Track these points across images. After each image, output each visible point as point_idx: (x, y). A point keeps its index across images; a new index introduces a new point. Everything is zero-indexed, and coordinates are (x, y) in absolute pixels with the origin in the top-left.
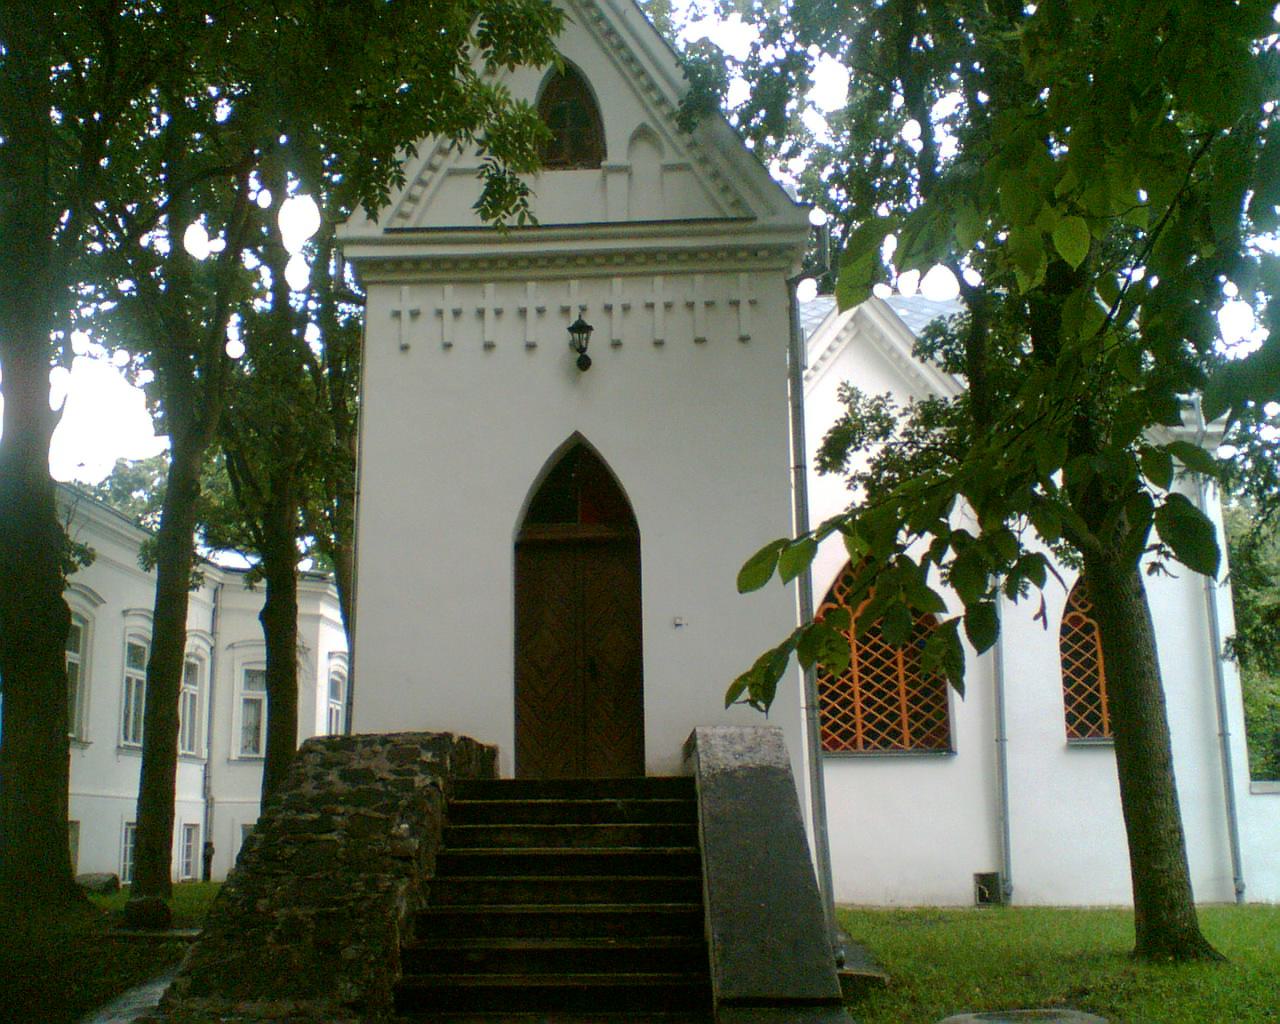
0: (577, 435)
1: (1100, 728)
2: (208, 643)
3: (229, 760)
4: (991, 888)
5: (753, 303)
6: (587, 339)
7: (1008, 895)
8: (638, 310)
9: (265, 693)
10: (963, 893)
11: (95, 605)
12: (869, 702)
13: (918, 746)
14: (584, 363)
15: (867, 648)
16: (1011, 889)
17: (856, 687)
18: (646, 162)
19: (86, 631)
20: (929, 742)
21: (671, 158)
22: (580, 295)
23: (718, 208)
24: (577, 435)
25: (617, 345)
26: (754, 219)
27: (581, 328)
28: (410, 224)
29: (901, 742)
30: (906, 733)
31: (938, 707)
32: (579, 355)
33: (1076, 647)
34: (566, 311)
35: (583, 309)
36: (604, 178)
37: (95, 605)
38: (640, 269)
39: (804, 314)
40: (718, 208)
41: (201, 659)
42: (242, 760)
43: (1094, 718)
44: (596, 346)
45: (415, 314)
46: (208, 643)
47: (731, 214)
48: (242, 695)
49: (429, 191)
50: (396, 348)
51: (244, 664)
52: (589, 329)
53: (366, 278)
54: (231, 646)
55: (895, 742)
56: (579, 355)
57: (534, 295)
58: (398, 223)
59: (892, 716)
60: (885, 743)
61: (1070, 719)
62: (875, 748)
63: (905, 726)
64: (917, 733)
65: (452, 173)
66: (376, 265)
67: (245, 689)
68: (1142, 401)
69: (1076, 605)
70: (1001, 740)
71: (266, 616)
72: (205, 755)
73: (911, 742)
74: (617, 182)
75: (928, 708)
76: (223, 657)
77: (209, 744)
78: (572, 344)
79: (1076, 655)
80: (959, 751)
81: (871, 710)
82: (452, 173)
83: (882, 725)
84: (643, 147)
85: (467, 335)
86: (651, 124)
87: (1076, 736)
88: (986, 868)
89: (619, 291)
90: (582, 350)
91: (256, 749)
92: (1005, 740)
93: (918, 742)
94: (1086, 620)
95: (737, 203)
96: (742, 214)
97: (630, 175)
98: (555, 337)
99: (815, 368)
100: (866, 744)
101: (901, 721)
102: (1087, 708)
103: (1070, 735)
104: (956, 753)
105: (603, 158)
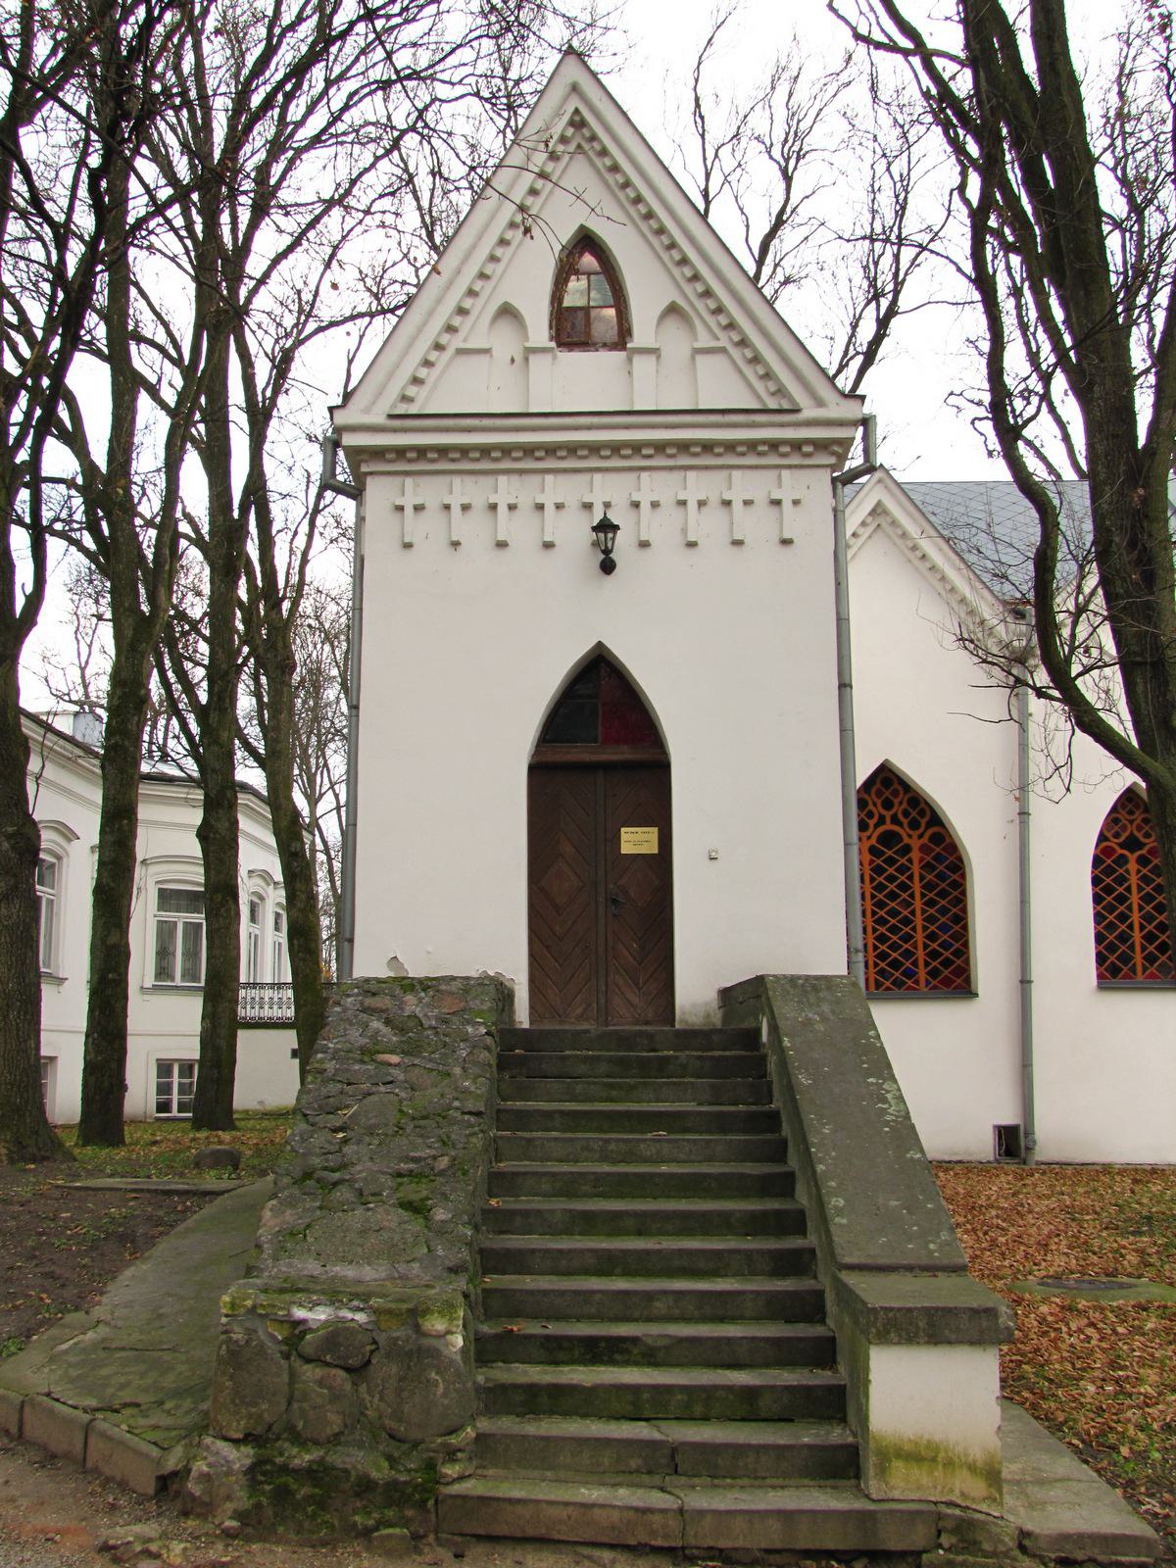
0: (600, 644)
1: (1133, 970)
4: (1012, 1141)
5: (796, 502)
6: (613, 539)
7: (1029, 1149)
8: (478, 513)
10: (983, 1146)
11: (69, 840)
13: (935, 987)
14: (608, 567)
15: (881, 879)
16: (1034, 1142)
18: (676, 342)
19: (60, 868)
20: (947, 982)
21: (704, 341)
22: (610, 490)
23: (758, 397)
24: (600, 644)
25: (644, 545)
26: (797, 411)
27: (606, 527)
28: (413, 409)
29: (917, 982)
30: (922, 973)
31: (957, 945)
32: (603, 556)
33: (890, 853)
34: (588, 506)
35: (607, 505)
36: (630, 360)
37: (69, 840)
38: (671, 462)
40: (758, 397)
43: (1126, 959)
44: (623, 545)
45: (419, 508)
47: (772, 404)
49: (436, 371)
50: (397, 546)
52: (616, 528)
53: (364, 469)
55: (910, 983)
56: (603, 556)
57: (557, 489)
58: (402, 409)
59: (908, 954)
60: (898, 984)
61: (1100, 959)
62: (888, 989)
64: (933, 973)
65: (460, 352)
66: (378, 453)
69: (1109, 835)
70: (1025, 982)
71: (204, 834)
73: (927, 983)
74: (643, 365)
75: (945, 945)
78: (596, 544)
79: (1108, 890)
80: (980, 992)
82: (460, 352)
83: (895, 964)
84: (672, 325)
85: (472, 530)
86: (681, 302)
87: (1105, 978)
88: (1009, 1117)
89: (656, 486)
90: (607, 552)
91: (196, 979)
93: (934, 982)
94: (1120, 851)
95: (781, 391)
96: (786, 406)
97: (659, 357)
98: (574, 533)
101: (917, 960)
102: (1156, 948)
103: (1100, 976)
104: (977, 995)
105: (628, 339)
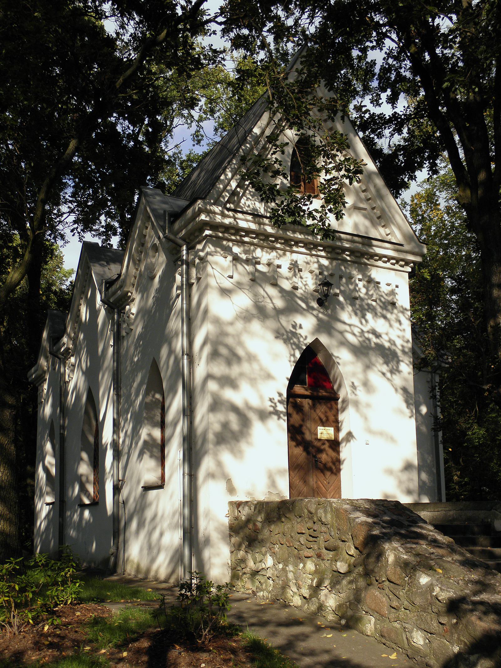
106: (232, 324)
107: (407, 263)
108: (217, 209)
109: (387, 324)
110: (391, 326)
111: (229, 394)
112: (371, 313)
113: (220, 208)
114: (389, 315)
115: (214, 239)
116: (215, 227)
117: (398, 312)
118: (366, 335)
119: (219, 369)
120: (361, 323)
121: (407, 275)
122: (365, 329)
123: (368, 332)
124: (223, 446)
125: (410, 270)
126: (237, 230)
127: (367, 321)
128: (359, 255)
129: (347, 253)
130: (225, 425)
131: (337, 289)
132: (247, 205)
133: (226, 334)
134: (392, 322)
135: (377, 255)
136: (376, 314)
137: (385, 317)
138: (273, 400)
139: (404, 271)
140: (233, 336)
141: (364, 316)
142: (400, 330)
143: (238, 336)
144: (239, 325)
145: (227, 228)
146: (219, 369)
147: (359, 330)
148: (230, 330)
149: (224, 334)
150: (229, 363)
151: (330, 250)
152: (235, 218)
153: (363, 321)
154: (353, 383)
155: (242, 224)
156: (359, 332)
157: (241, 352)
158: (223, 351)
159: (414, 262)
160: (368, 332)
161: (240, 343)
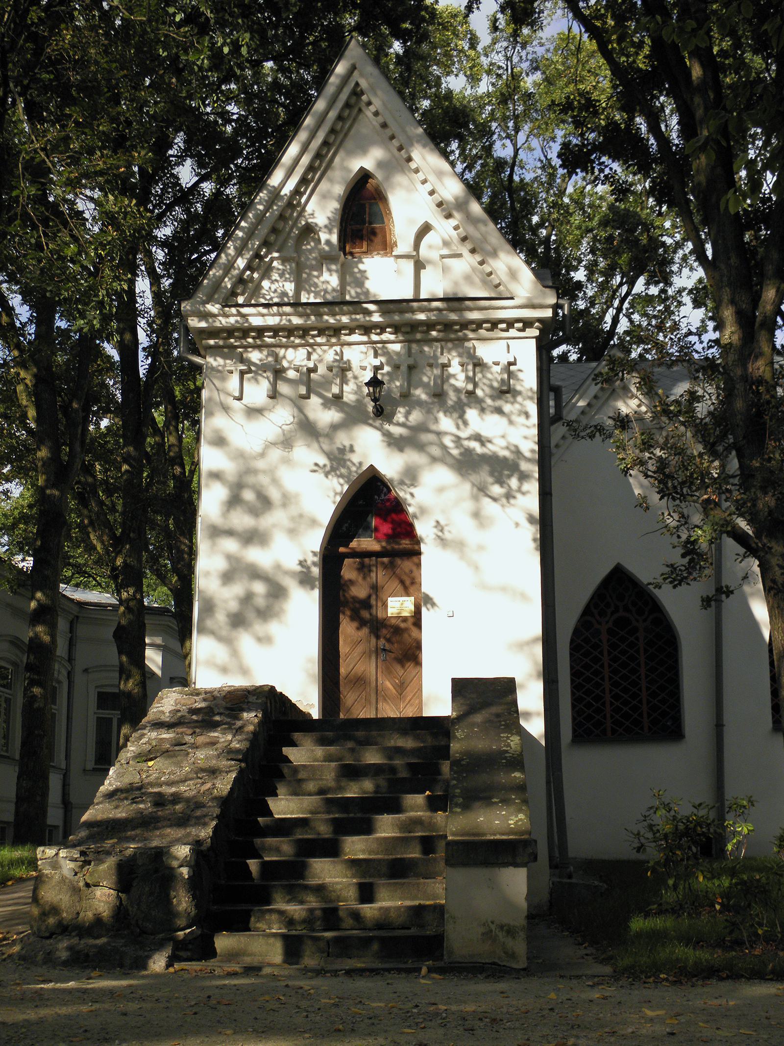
2: (66, 668)
3: (84, 770)
9: (537, 469)
12: (616, 697)
17: (607, 685)
39: (220, 441)
41: (59, 682)
42: (94, 770)
46: (66, 668)
48: (95, 713)
51: (97, 687)
54: (86, 671)
63: (644, 701)
67: (98, 709)
68: (137, 94)
70: (719, 726)
72: (63, 766)
76: (79, 679)
77: (67, 757)
81: (618, 704)
92: (723, 725)
99: (557, 446)
100: (614, 731)
106: (262, 455)
107: (527, 323)
108: (213, 308)
109: (504, 421)
110: (511, 422)
111: (256, 555)
112: (476, 408)
113: (218, 306)
114: (507, 408)
115: (226, 350)
116: (213, 333)
117: (524, 399)
118: (466, 443)
119: (241, 520)
120: (458, 427)
121: (533, 342)
122: (463, 435)
123: (469, 439)
124: (241, 630)
125: (536, 333)
126: (245, 332)
127: (466, 423)
128: (408, 329)
129: (388, 330)
130: (247, 599)
131: (46, 481)
132: (273, 289)
133: (255, 472)
134: (514, 418)
135: (472, 322)
136: (483, 410)
137: (499, 411)
138: (304, 564)
139: (527, 338)
140: (264, 472)
141: (462, 416)
142: (528, 427)
143: (271, 472)
144: (276, 454)
145: (230, 332)
146: (241, 520)
147: (453, 438)
148: (261, 464)
149: (250, 471)
150: (255, 512)
151: (408, 329)
152: (239, 314)
153: (460, 422)
154: (438, 522)
155: (256, 321)
156: (453, 441)
157: (274, 494)
158: (248, 495)
159: (540, 320)
160: (469, 439)
161: (275, 481)
